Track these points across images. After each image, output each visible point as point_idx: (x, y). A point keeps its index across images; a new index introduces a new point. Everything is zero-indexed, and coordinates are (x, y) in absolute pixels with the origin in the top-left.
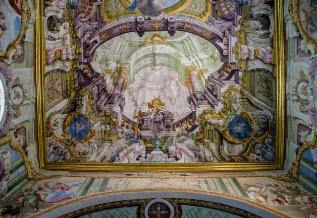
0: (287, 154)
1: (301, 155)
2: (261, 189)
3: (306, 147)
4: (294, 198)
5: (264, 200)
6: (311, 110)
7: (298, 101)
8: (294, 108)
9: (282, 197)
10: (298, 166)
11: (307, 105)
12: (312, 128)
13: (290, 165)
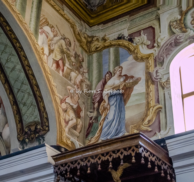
0: (110, 24)
1: (119, 45)
2: (54, 36)
3: (132, 48)
4: (71, 70)
5: (47, 54)
6: (176, 39)
7: (181, 13)
8: (170, 11)
9: (63, 62)
10: (105, 47)
11: (181, 29)
12: (155, 48)
13: (100, 35)
